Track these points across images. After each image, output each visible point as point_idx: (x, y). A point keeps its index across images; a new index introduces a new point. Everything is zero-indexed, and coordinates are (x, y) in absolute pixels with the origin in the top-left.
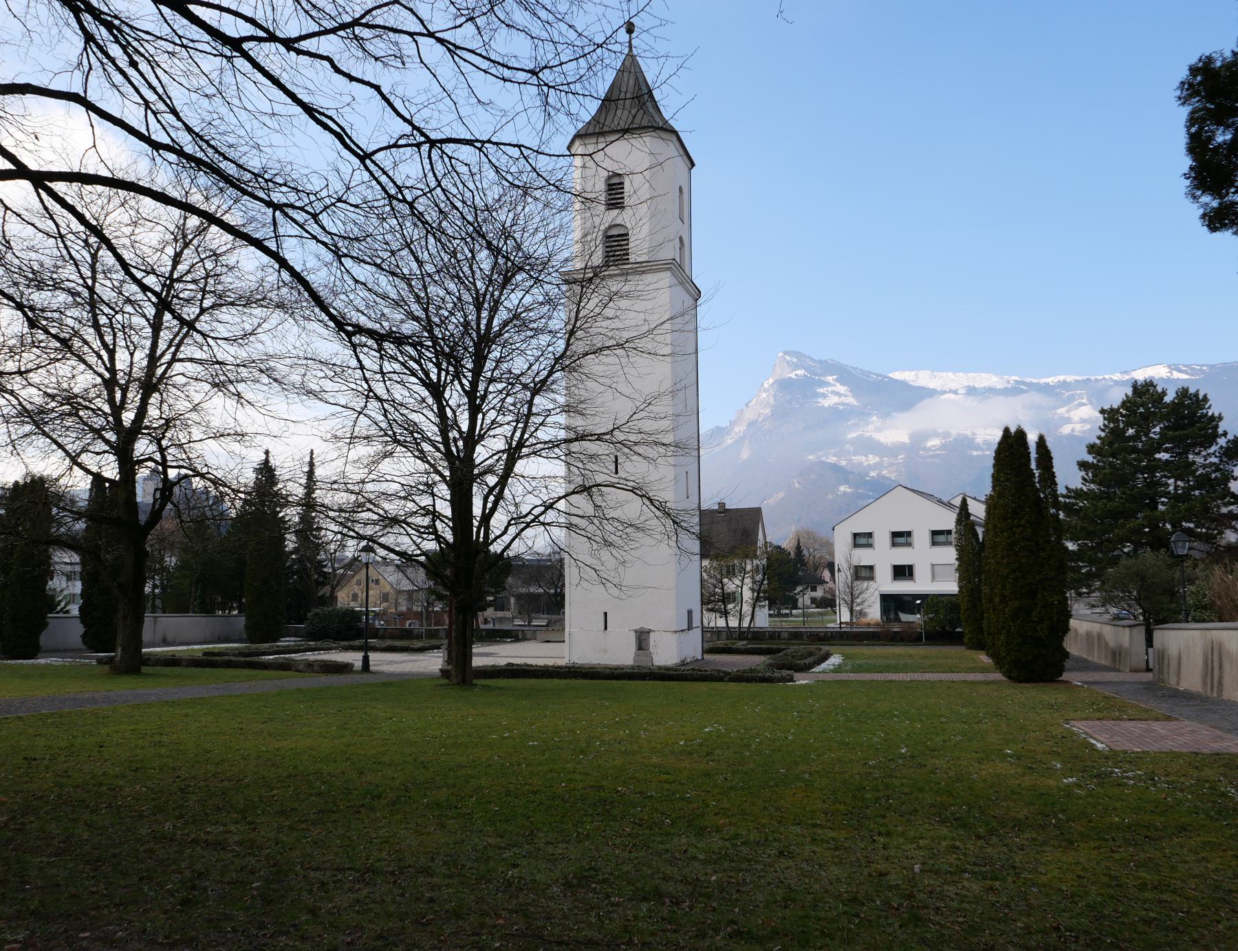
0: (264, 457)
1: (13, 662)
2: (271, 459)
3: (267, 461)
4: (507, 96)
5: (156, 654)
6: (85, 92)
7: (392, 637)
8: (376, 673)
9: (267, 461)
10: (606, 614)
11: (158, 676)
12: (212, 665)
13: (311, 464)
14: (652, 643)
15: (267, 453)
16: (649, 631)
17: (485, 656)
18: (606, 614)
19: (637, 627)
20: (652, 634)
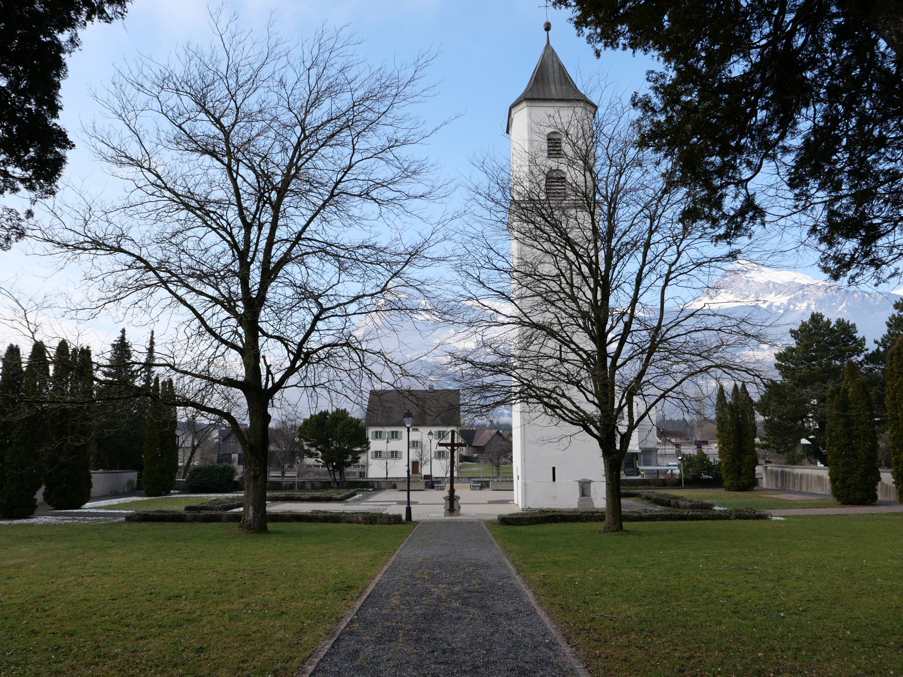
0: (120, 334)
1: (15, 522)
2: (126, 337)
3: (123, 338)
4: (239, 222)
5: (831, 509)
6: (278, 241)
7: (314, 488)
8: (417, 523)
9: (123, 338)
10: (554, 469)
11: (299, 534)
12: (195, 519)
13: (152, 343)
14: (592, 491)
15: (123, 331)
16: (590, 482)
17: (274, 508)
18: (554, 469)
19: (580, 479)
20: (592, 484)
